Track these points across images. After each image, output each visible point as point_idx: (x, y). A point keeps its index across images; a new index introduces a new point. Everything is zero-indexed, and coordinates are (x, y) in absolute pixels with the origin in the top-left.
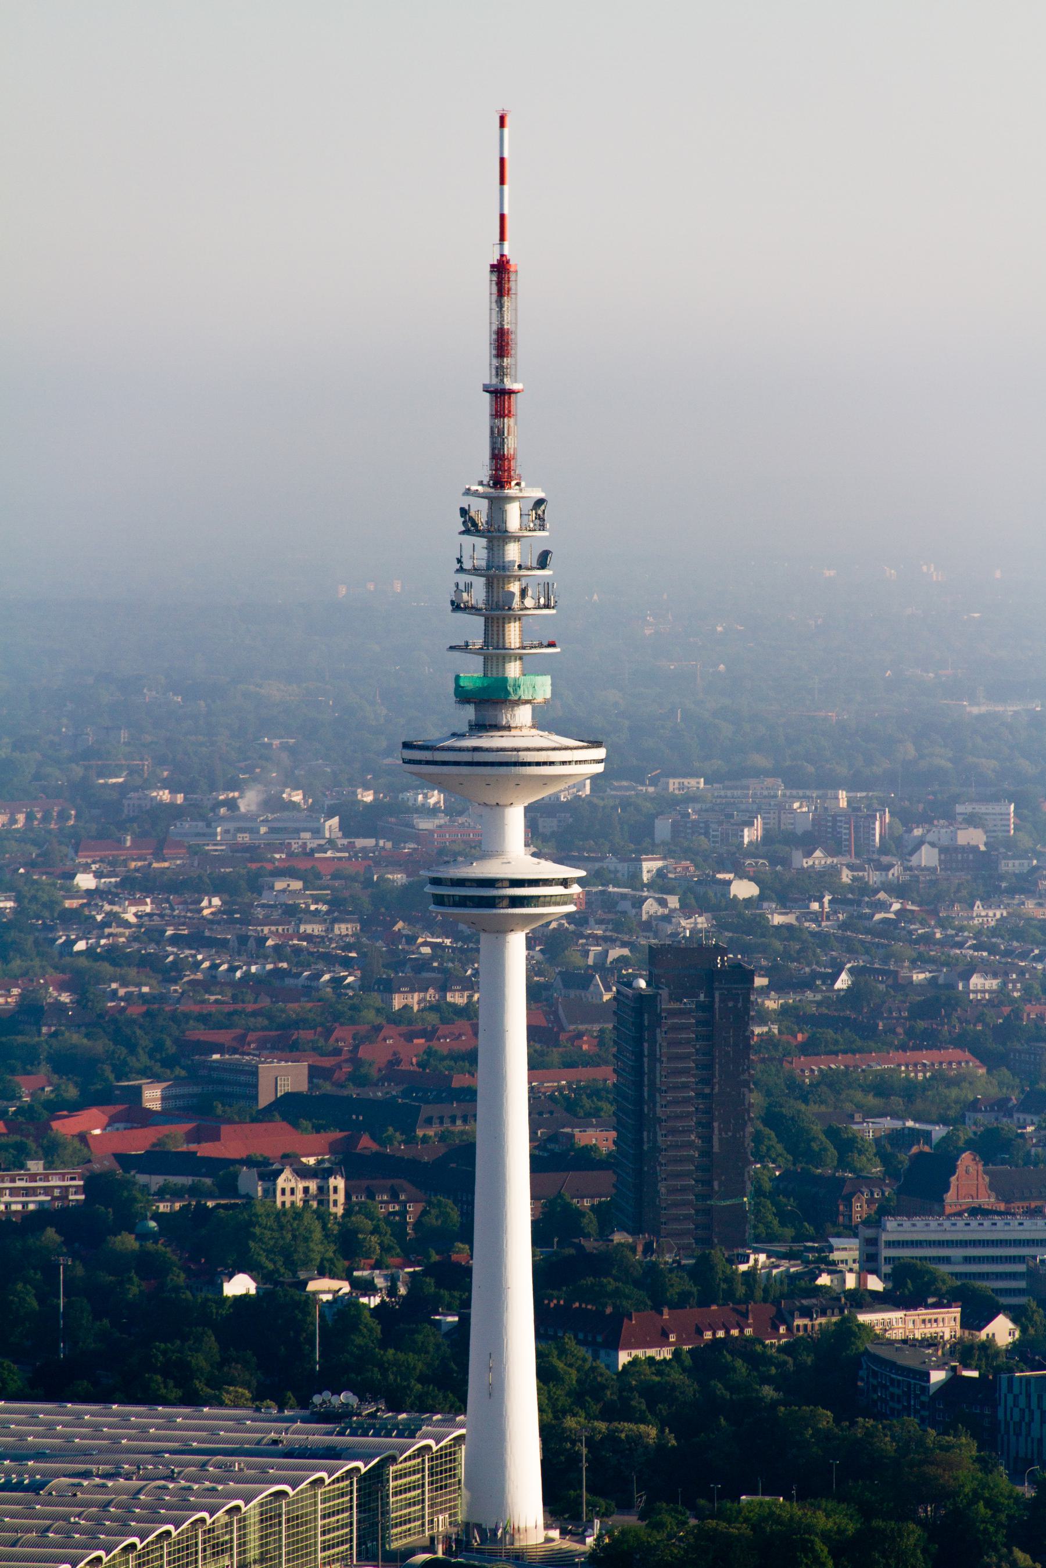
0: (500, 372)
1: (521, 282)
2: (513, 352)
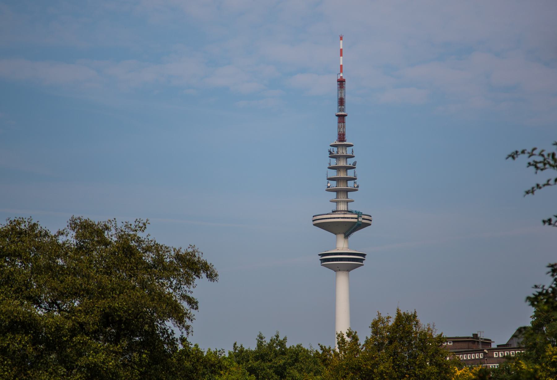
1: (347, 85)
2: (344, 105)
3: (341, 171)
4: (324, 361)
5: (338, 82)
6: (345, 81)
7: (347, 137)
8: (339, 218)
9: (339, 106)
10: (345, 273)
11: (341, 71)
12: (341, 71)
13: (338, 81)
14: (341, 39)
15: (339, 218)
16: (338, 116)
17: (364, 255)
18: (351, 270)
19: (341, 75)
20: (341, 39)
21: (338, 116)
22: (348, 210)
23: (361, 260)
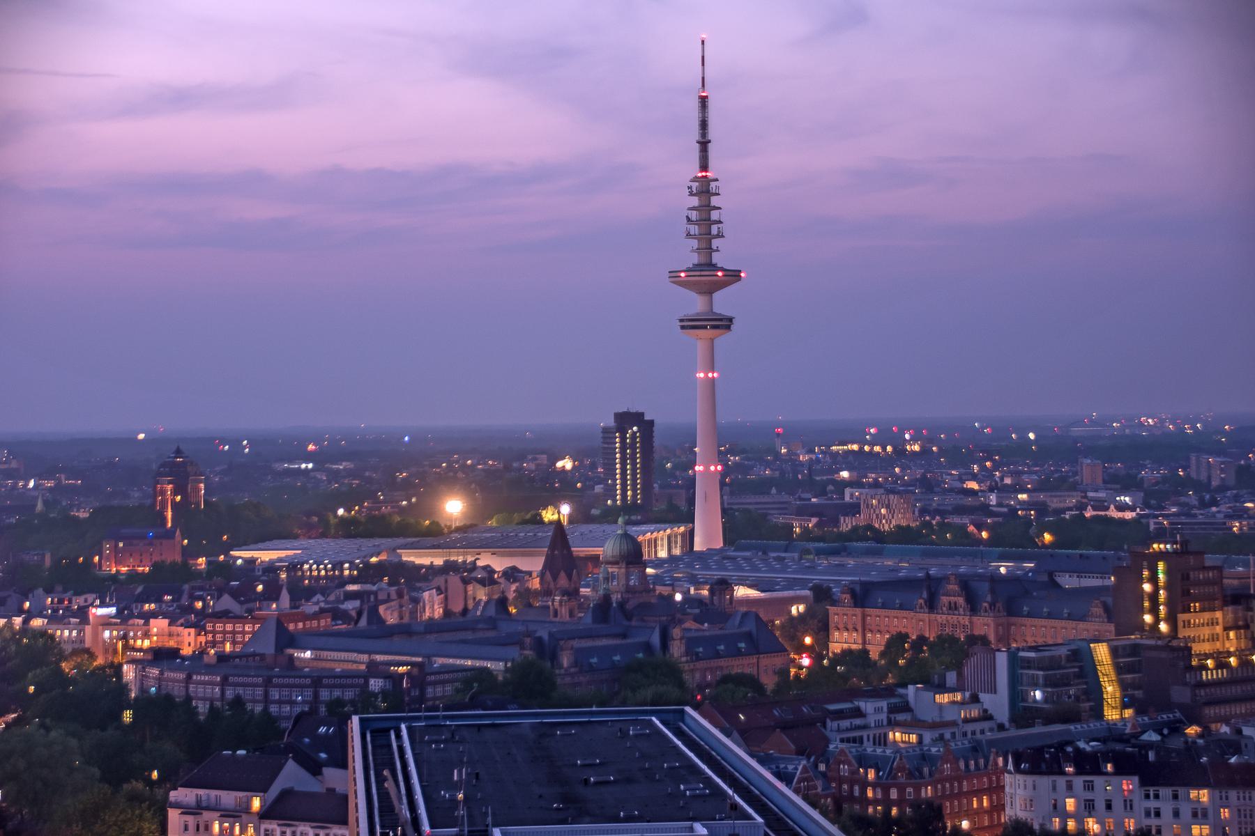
1: (711, 104)
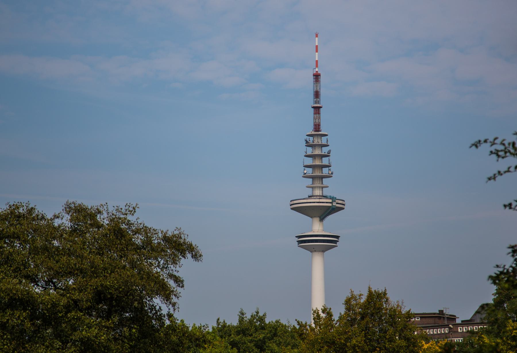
0: (316, 102)
1: (322, 79)
2: (319, 97)
3: (317, 159)
4: (301, 335)
5: (313, 76)
6: (320, 76)
7: (322, 127)
8: (314, 202)
9: (315, 98)
10: (320, 253)
11: (317, 66)
12: (317, 66)
13: (314, 75)
14: (317, 36)
15: (314, 202)
16: (313, 107)
17: (338, 237)
18: (326, 251)
19: (317, 70)
20: (317, 36)
21: (313, 107)
22: (323, 195)
23: (335, 242)
